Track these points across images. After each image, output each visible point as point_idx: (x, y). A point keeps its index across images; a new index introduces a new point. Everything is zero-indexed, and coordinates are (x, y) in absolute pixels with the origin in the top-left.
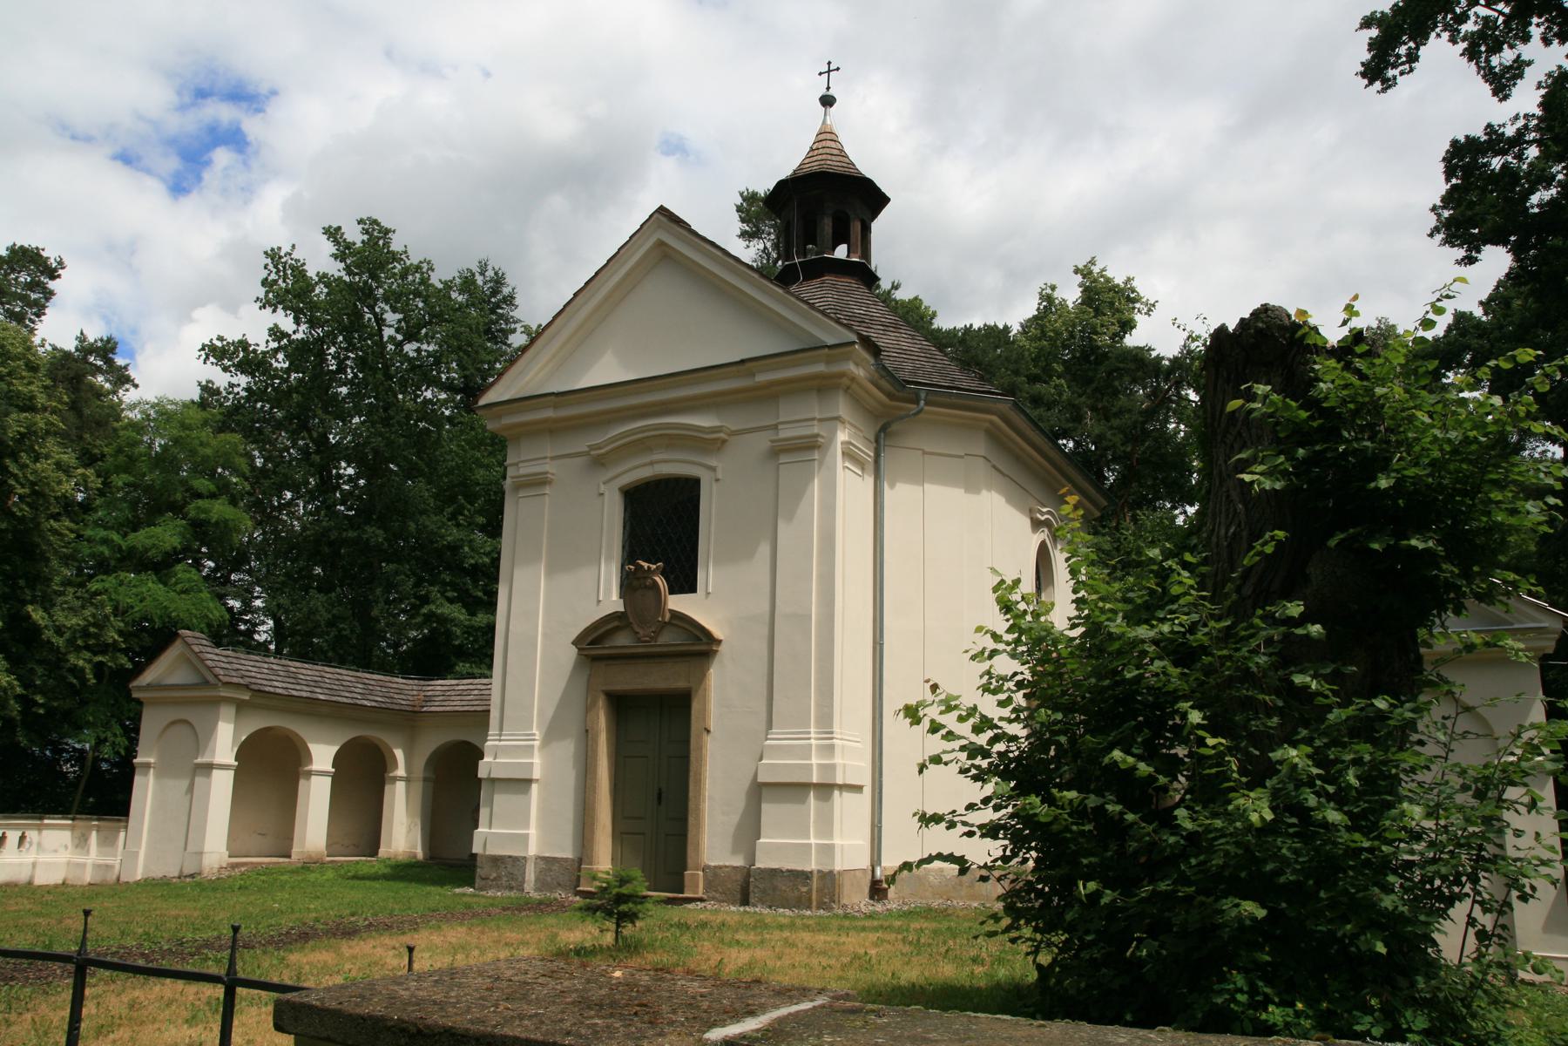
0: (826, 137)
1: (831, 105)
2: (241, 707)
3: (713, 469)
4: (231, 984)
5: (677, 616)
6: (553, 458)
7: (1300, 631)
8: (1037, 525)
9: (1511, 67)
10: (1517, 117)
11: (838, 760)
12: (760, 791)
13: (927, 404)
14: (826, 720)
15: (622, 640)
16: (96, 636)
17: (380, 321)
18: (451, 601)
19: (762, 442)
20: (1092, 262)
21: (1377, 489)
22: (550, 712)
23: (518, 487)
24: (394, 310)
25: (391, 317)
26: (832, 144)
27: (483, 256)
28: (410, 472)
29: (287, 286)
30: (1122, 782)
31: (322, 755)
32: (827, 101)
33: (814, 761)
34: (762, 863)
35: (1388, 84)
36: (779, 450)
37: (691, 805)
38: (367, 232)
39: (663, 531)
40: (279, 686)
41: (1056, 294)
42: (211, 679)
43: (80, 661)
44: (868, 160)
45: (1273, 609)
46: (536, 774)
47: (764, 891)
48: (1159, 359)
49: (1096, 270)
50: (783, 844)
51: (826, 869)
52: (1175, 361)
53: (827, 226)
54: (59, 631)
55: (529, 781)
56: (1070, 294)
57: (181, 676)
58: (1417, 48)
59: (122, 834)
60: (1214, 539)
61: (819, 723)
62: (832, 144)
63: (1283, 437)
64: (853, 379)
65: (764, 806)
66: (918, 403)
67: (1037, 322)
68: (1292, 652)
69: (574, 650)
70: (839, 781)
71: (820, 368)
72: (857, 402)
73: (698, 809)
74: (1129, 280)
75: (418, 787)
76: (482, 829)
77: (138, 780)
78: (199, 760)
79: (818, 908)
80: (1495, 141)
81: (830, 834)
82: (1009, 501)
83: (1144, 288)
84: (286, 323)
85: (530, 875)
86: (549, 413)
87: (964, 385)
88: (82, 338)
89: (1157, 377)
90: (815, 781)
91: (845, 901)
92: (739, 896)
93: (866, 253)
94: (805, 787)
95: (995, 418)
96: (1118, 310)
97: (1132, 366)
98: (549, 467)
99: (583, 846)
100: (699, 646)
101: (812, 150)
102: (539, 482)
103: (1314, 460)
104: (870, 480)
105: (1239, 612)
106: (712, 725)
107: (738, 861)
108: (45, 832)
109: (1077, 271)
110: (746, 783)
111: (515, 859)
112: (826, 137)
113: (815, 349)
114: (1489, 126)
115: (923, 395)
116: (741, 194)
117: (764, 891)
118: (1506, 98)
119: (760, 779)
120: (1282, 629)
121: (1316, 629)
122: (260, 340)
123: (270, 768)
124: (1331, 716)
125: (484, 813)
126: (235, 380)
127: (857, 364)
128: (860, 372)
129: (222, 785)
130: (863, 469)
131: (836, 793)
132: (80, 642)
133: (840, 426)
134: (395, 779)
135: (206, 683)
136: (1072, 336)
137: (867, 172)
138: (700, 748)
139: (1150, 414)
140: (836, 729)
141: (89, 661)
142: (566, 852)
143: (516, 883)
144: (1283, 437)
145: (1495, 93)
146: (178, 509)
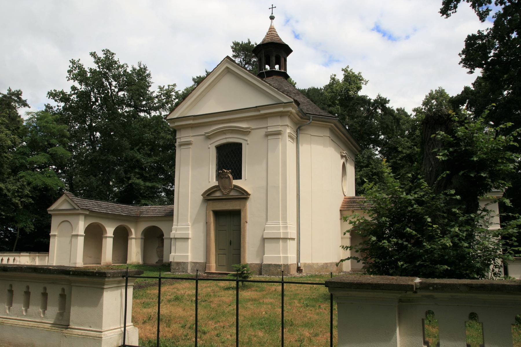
0: (272, 30)
2: (86, 216)
3: (247, 141)
5: (235, 186)
6: (192, 136)
7: (454, 197)
8: (342, 157)
9: (485, 11)
10: (488, 29)
11: (289, 231)
12: (264, 240)
13: (313, 120)
14: (285, 219)
16: (21, 192)
17: (110, 84)
18: (138, 178)
19: (263, 132)
20: (348, 67)
21: (473, 160)
23: (180, 145)
24: (115, 81)
25: (114, 83)
26: (274, 32)
27: (139, 61)
28: (122, 136)
29: (79, 73)
30: (409, 237)
31: (110, 231)
32: (272, 18)
33: (281, 231)
34: (265, 262)
35: (448, 16)
36: (267, 135)
37: (242, 245)
38: (105, 54)
39: (230, 159)
40: (96, 209)
41: (336, 78)
42: (77, 208)
43: (16, 200)
44: (286, 38)
45: (446, 191)
47: (266, 271)
48: (370, 99)
49: (349, 70)
50: (273, 256)
51: (286, 263)
52: (375, 101)
53: (273, 59)
54: (9, 190)
55: (188, 238)
56: (340, 77)
57: (65, 206)
58: (457, 4)
59: (47, 258)
60: (425, 171)
62: (274, 32)
63: (445, 145)
64: (291, 113)
65: (266, 245)
66: (309, 120)
67: (330, 86)
68: (451, 202)
70: (289, 237)
71: (281, 109)
72: (292, 120)
73: (244, 246)
74: (360, 73)
75: (139, 241)
77: (52, 240)
78: (74, 233)
80: (481, 36)
81: (287, 253)
83: (364, 76)
84: (77, 84)
85: (189, 268)
86: (191, 122)
87: (323, 114)
88: (10, 90)
89: (369, 105)
90: (282, 237)
91: (291, 273)
93: (285, 69)
95: (332, 125)
96: (356, 83)
97: (361, 102)
100: (244, 196)
101: (268, 34)
102: (189, 144)
103: (455, 151)
104: (295, 144)
105: (437, 192)
107: (258, 262)
108: (21, 258)
109: (343, 70)
110: (259, 238)
111: (184, 263)
112: (272, 30)
113: (280, 104)
114: (479, 31)
115: (311, 117)
117: (266, 271)
118: (483, 21)
120: (449, 197)
121: (458, 197)
122: (68, 91)
123: (94, 235)
124: (460, 219)
126: (59, 104)
128: (294, 111)
129: (81, 241)
131: (288, 241)
132: (16, 194)
134: (132, 238)
135: (75, 209)
138: (244, 227)
139: (367, 118)
141: (19, 200)
142: (201, 259)
143: (185, 270)
144: (445, 145)
145: (480, 19)
146: (44, 150)
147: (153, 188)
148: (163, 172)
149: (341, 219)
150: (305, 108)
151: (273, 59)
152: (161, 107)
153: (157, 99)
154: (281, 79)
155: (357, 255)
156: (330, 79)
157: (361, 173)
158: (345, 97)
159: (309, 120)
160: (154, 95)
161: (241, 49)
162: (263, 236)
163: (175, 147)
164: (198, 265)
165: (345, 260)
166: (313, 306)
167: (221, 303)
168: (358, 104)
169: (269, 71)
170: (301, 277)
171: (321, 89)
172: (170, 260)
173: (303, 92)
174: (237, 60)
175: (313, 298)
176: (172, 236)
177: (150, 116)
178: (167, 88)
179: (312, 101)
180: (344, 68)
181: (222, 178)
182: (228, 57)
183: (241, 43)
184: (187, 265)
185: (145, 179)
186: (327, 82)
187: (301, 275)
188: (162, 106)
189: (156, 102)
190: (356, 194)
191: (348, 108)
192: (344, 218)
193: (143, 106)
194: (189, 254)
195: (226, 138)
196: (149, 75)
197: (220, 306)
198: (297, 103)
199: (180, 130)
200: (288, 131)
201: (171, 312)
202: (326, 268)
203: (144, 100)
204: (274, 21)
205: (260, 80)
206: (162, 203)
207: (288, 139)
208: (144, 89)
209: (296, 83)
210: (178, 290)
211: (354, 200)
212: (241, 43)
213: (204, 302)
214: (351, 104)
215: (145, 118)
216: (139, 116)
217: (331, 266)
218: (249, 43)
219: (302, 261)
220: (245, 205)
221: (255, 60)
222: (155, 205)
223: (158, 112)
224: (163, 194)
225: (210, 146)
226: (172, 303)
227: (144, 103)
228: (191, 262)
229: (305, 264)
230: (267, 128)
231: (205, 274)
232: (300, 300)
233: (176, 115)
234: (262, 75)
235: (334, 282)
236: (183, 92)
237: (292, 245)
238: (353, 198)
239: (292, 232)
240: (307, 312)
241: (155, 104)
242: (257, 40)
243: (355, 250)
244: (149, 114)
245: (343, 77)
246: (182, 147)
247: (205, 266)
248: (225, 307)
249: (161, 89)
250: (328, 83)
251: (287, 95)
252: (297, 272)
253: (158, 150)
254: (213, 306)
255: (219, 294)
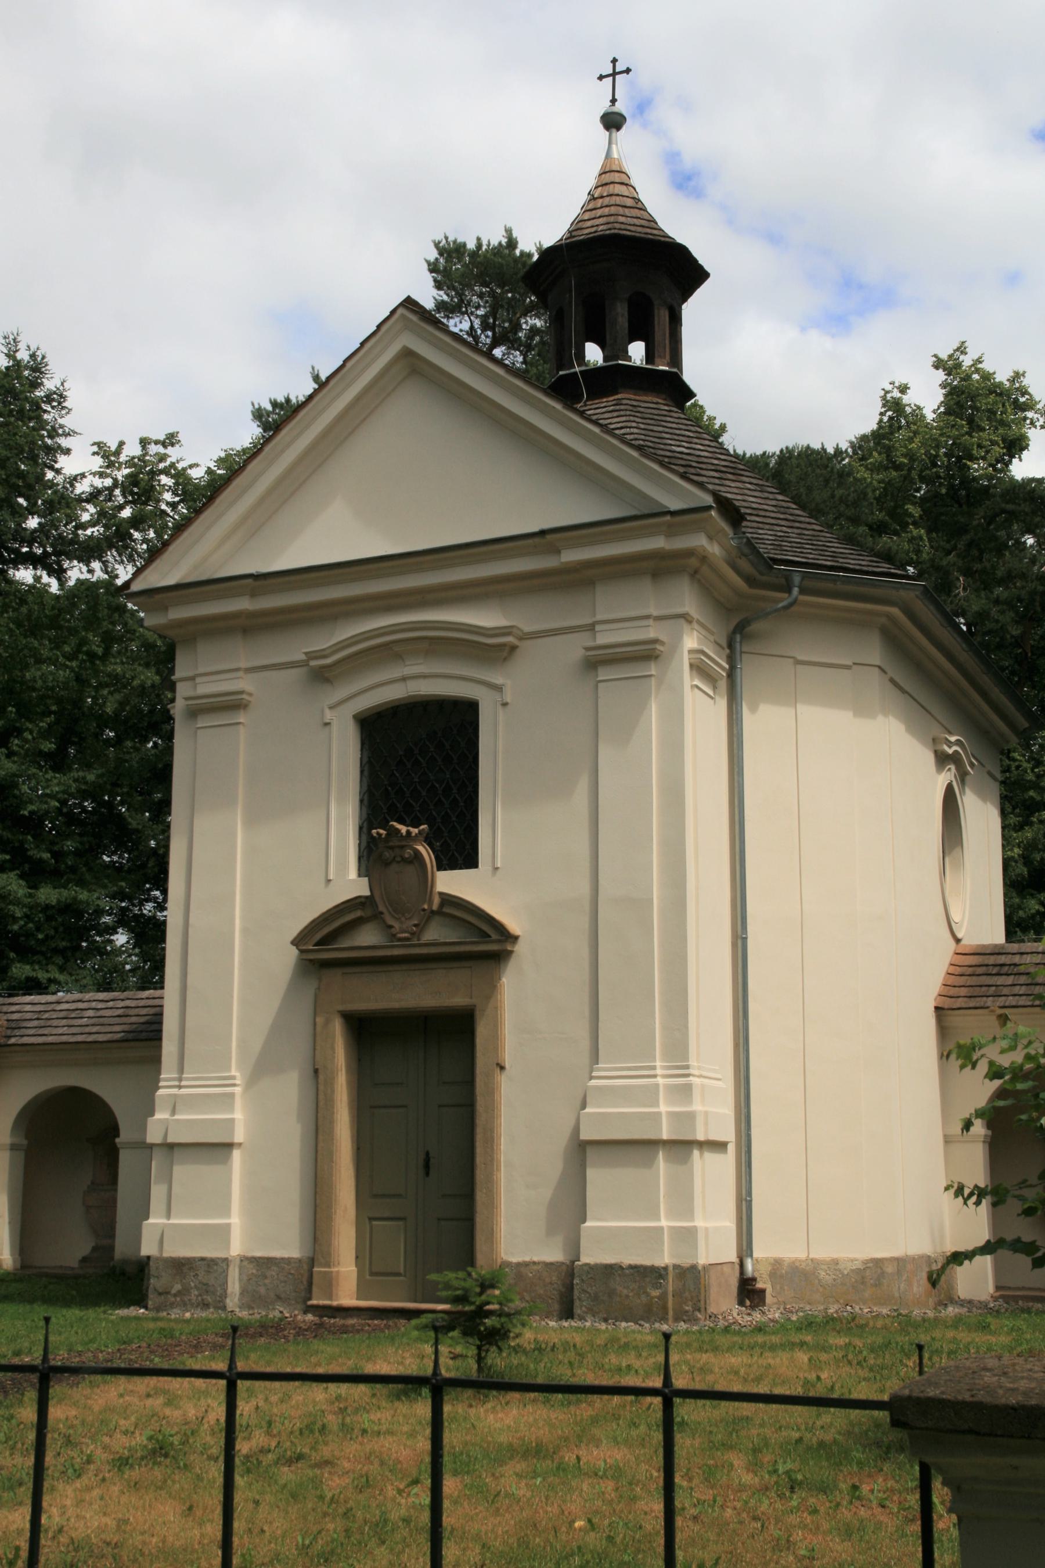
0: (612, 178)
1: (618, 128)
3: (499, 688)
4: (232, 1379)
5: (448, 900)
6: (249, 670)
8: (942, 760)
11: (697, 1106)
12: (582, 1151)
13: (803, 591)
14: (678, 1051)
15: (368, 937)
19: (574, 648)
20: (962, 349)
22: (257, 1045)
23: (194, 713)
27: (10, 329)
32: (612, 122)
33: (663, 1108)
34: (589, 1257)
36: (596, 662)
39: (423, 777)
41: (906, 399)
44: (679, 222)
46: (239, 1137)
47: (596, 1298)
49: (967, 361)
50: (618, 1229)
51: (686, 1262)
53: (620, 315)
55: (229, 1146)
56: (927, 397)
61: (667, 1055)
64: (704, 559)
65: (591, 1173)
66: (788, 590)
67: (879, 439)
69: (294, 951)
70: (701, 1137)
72: (707, 590)
74: (1017, 376)
76: (155, 1220)
79: (677, 1319)
82: (911, 729)
87: (852, 563)
90: (665, 1137)
91: (712, 1309)
92: (556, 1306)
93: (676, 359)
94: (646, 1147)
95: (895, 611)
96: (1003, 423)
97: (1026, 507)
98: (243, 683)
99: (315, 1239)
100: (487, 945)
101: (592, 198)
102: (232, 704)
104: (722, 703)
106: (508, 1059)
107: (553, 1254)
109: (938, 364)
110: (559, 1142)
112: (612, 178)
113: (652, 516)
115: (797, 579)
116: (437, 245)
117: (596, 1298)
119: (584, 1136)
125: (157, 1192)
127: (710, 538)
128: (714, 550)
130: (715, 688)
131: (696, 1153)
133: (686, 627)
136: (933, 461)
137: (679, 240)
138: (492, 1091)
140: (693, 1062)
142: (288, 1246)
143: (212, 1296)
147: (71, 909)
148: (124, 836)
149: (944, 1056)
150: (766, 535)
151: (620, 315)
152: (111, 546)
153: (92, 509)
154: (652, 403)
155: (1025, 1230)
156: (878, 407)
157: (1028, 834)
158: (951, 487)
159: (788, 590)
160: (82, 488)
161: (471, 271)
162: (576, 1130)
163: (169, 719)
164: (273, 1272)
165: (969, 1255)
166: (824, 1489)
167: (374, 1468)
168: (1012, 515)
169: (597, 371)
170: (760, 1329)
171: (838, 452)
172: (145, 1251)
173: (757, 465)
174: (459, 325)
175: (822, 1444)
176: (153, 1136)
177: (62, 582)
178: (137, 451)
179: (802, 507)
180: (944, 356)
181: (387, 864)
182: (409, 303)
183: (471, 245)
184: (225, 1272)
185: (35, 874)
186: (863, 419)
187: (757, 1316)
188: (118, 538)
189: (85, 517)
190: (1010, 934)
191: (967, 538)
192: (956, 1051)
193: (32, 538)
194: (235, 1220)
195: (404, 679)
196: (57, 399)
197: (368, 1484)
198: (733, 514)
199: (191, 640)
200: (691, 641)
201: (122, 1522)
202: (878, 1284)
203: (31, 511)
204: (621, 135)
205: (559, 406)
206: (108, 981)
207: (688, 679)
208: (33, 459)
209: (723, 428)
210: (169, 1403)
211: (1002, 959)
212: (471, 245)
213: (290, 1462)
214: (979, 518)
215: (37, 591)
216: (10, 582)
217: (899, 1272)
218: (512, 243)
219: (763, 1250)
220: (492, 987)
221: (538, 323)
222: (83, 989)
223: (96, 565)
224: (121, 938)
225: (329, 715)
226: (135, 1474)
227: (33, 523)
228: (243, 1259)
229: (777, 1262)
230: (591, 628)
231: (310, 1317)
232: (756, 1451)
233: (167, 573)
234: (571, 389)
235: (940, 1404)
236: (209, 472)
237: (714, 1174)
238: (996, 951)
239: (715, 1117)
240: (793, 1519)
241: (84, 526)
242: (540, 231)
243: (1016, 1206)
244: (59, 573)
245: (939, 396)
246: (203, 722)
247: (305, 1276)
248: (390, 1492)
249: (109, 455)
250: (868, 425)
251: (684, 476)
252: (741, 1303)
253: (97, 736)
254: (334, 1484)
255: (365, 1420)
